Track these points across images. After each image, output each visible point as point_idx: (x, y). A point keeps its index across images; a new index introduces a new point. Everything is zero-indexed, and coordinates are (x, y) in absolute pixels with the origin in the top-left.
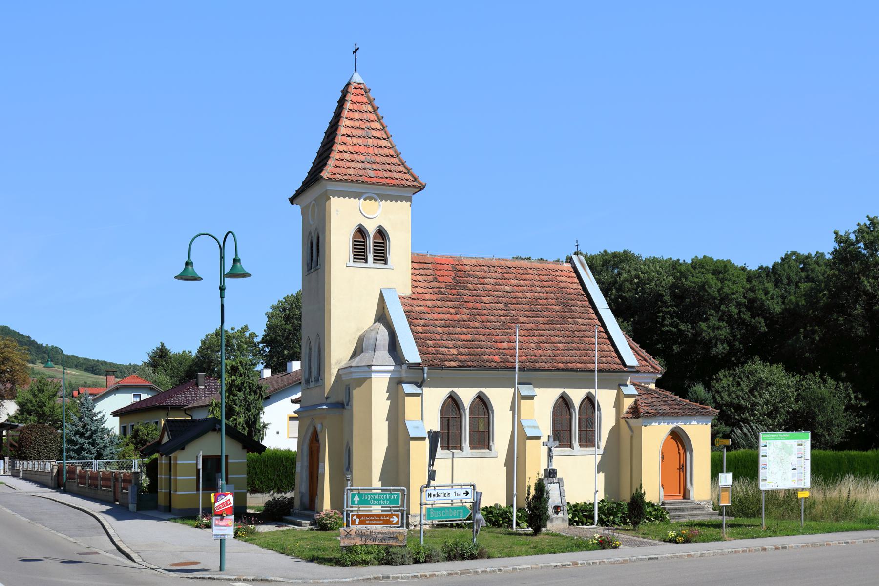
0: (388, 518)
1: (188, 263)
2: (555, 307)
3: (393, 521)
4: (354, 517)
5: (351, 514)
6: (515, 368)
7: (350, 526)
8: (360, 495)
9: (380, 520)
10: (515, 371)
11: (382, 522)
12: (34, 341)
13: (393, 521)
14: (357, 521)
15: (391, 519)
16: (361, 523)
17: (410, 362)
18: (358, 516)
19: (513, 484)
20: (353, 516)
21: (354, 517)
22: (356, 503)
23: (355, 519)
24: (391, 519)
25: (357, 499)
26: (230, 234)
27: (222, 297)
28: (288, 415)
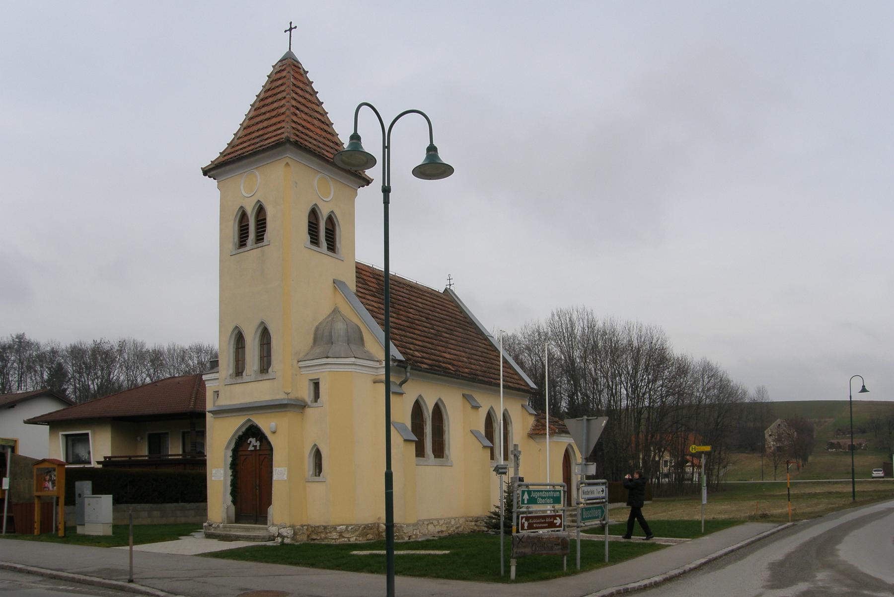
0: (552, 520)
1: (432, 150)
2: (458, 329)
3: (557, 523)
4: (524, 520)
5: (521, 516)
6: (500, 385)
7: (520, 531)
8: (529, 492)
9: (545, 523)
10: (500, 387)
11: (547, 525)
12: (383, 192)
13: (557, 523)
14: (526, 524)
15: (555, 521)
16: (530, 527)
17: (397, 358)
18: (527, 519)
19: (408, 555)
20: (522, 518)
21: (524, 520)
22: (526, 502)
23: (524, 523)
24: (555, 521)
25: (526, 497)
26: (365, 111)
27: (386, 202)
28: (18, 439)
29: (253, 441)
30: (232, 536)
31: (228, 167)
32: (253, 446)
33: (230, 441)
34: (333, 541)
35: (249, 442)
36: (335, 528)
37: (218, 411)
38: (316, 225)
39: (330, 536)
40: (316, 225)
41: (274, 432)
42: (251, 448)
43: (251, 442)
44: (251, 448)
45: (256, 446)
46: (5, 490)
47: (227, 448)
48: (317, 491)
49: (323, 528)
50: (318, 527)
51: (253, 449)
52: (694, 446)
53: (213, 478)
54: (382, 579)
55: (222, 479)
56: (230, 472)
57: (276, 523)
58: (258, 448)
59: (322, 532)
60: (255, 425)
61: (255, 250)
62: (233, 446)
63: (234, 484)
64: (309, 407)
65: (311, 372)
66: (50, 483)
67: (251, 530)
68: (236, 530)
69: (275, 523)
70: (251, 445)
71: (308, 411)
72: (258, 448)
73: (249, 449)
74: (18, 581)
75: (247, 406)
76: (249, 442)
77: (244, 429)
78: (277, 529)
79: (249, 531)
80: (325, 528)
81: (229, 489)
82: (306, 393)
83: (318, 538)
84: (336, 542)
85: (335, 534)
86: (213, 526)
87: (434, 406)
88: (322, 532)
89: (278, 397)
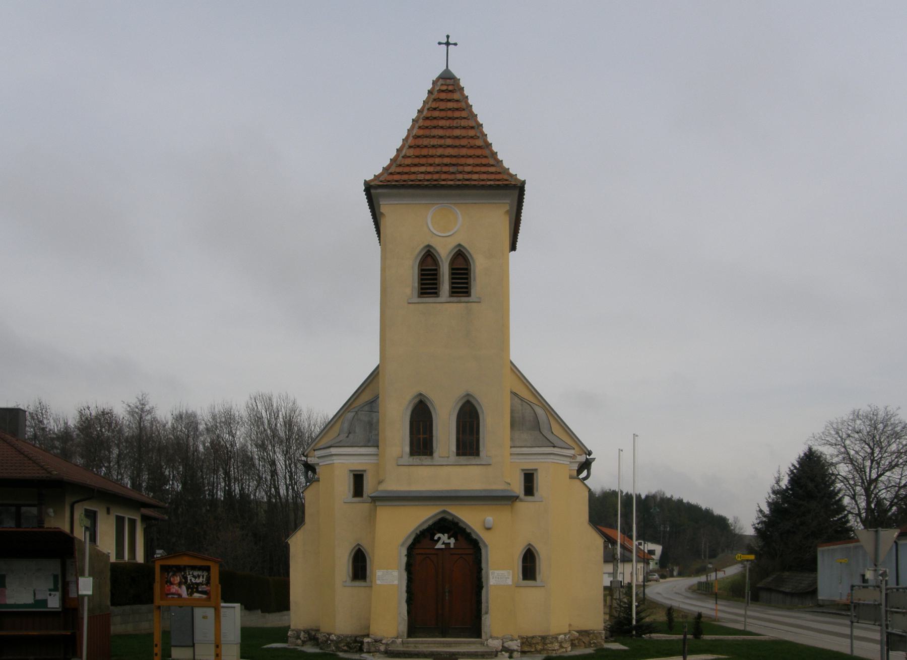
29: (444, 540)
30: (442, 653)
31: (402, 191)
32: (444, 543)
33: (409, 537)
34: (554, 652)
35: (436, 538)
36: (557, 638)
37: (379, 497)
38: (467, 269)
39: (550, 647)
40: (467, 269)
41: (489, 529)
42: (439, 546)
43: (439, 538)
44: (439, 546)
45: (449, 543)
46: (83, 596)
47: (402, 545)
48: (531, 594)
49: (540, 638)
50: (533, 637)
51: (443, 546)
52: (739, 555)
53: (378, 582)
54: (849, 640)
55: (396, 582)
56: (405, 575)
57: (496, 636)
58: (452, 546)
59: (538, 643)
60: (450, 518)
61: (455, 304)
62: (410, 541)
63: (409, 591)
64: (521, 500)
65: (523, 461)
66: (184, 588)
67: (453, 645)
68: (426, 645)
69: (495, 635)
70: (441, 542)
71: (519, 505)
72: (452, 546)
73: (436, 547)
74: (766, 635)
75: (443, 495)
76: (436, 538)
77: (430, 522)
78: (501, 642)
79: (450, 647)
80: (544, 638)
81: (404, 596)
82: (518, 487)
83: (532, 650)
84: (556, 653)
85: (556, 644)
86: (383, 642)
87: (454, 489)
88: (538, 643)
89: (494, 487)
